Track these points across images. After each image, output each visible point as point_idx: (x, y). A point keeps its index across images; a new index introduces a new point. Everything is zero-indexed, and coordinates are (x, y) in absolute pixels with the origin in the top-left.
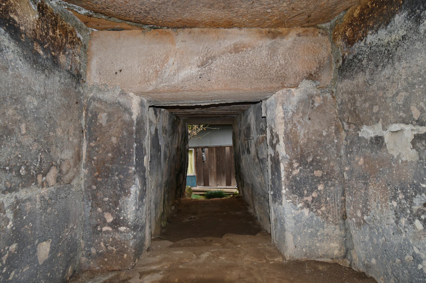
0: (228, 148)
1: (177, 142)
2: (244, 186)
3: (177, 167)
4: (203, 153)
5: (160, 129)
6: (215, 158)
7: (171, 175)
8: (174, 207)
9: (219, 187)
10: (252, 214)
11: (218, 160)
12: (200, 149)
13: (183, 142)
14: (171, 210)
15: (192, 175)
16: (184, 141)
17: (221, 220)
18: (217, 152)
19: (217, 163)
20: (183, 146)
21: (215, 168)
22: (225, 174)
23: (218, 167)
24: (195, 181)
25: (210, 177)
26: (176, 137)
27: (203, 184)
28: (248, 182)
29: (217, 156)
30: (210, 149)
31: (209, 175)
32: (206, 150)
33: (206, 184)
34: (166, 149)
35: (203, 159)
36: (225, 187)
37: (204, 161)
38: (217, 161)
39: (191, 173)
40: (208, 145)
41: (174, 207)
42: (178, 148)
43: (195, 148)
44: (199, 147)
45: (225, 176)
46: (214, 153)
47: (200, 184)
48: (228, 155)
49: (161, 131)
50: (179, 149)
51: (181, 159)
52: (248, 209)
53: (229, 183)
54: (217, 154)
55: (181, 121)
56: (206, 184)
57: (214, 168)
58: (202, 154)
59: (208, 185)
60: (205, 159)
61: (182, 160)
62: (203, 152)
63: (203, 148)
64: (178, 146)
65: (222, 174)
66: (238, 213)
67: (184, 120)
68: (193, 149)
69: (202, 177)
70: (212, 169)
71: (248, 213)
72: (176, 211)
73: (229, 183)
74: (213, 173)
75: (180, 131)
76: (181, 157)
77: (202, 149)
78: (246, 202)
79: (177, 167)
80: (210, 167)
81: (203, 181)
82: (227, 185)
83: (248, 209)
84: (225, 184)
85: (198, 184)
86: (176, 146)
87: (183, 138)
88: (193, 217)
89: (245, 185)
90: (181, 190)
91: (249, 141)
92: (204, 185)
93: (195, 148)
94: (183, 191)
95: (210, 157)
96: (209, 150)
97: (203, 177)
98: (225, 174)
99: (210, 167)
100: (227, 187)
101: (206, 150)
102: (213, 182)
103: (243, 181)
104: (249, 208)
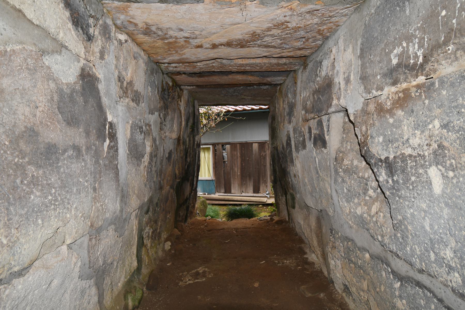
0: (257, 144)
1: (175, 127)
2: (294, 207)
3: (177, 172)
4: (224, 151)
5: (108, 80)
6: (239, 158)
7: (161, 188)
8: (169, 243)
9: (243, 194)
10: (316, 266)
11: (243, 160)
12: (220, 146)
13: (189, 130)
14: (164, 250)
15: (210, 178)
16: (193, 130)
17: (256, 285)
18: (241, 149)
19: (242, 164)
20: (189, 137)
21: (239, 171)
22: (252, 178)
23: (243, 169)
24: (213, 187)
25: (232, 182)
26: (172, 119)
27: (223, 190)
28: (310, 202)
29: (242, 155)
30: (233, 145)
31: (232, 180)
32: (228, 147)
33: (228, 190)
34: (139, 137)
35: (224, 159)
36: (252, 195)
37: (224, 162)
38: (241, 161)
39: (209, 176)
40: (230, 140)
41: (169, 243)
42: (179, 139)
43: (214, 145)
44: (218, 144)
45: (252, 180)
46: (238, 150)
47: (220, 190)
48: (256, 154)
49: (115, 89)
50: (181, 142)
51: (186, 158)
52: (305, 253)
53: (256, 190)
54: (242, 152)
55: (185, 92)
56: (228, 190)
57: (237, 170)
58: (223, 153)
59: (230, 193)
60: (226, 159)
61: (188, 160)
62: (224, 149)
63: (223, 145)
64: (179, 137)
65: (248, 178)
66: (287, 262)
67: (190, 92)
68: (211, 146)
69: (223, 182)
70: (235, 172)
71: (306, 262)
72: (173, 252)
73: (256, 190)
74: (236, 177)
75: (182, 109)
76: (186, 155)
77: (223, 146)
78: (296, 234)
79: (177, 172)
80: (233, 169)
81: (223, 186)
82: (254, 192)
83: (305, 253)
84: (252, 191)
85: (218, 190)
86: (174, 136)
87: (190, 124)
88: (201, 270)
89: (297, 206)
90: (188, 208)
91: (325, 118)
92: (225, 192)
93: (214, 145)
94: (190, 209)
95: (232, 156)
96: (231, 148)
97: (223, 180)
98: (252, 178)
99: (232, 168)
100: (255, 195)
101: (228, 147)
102: (237, 188)
103: (293, 198)
104: (307, 250)
